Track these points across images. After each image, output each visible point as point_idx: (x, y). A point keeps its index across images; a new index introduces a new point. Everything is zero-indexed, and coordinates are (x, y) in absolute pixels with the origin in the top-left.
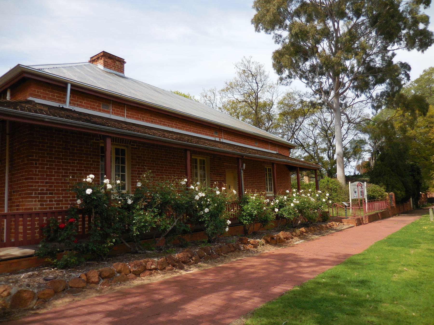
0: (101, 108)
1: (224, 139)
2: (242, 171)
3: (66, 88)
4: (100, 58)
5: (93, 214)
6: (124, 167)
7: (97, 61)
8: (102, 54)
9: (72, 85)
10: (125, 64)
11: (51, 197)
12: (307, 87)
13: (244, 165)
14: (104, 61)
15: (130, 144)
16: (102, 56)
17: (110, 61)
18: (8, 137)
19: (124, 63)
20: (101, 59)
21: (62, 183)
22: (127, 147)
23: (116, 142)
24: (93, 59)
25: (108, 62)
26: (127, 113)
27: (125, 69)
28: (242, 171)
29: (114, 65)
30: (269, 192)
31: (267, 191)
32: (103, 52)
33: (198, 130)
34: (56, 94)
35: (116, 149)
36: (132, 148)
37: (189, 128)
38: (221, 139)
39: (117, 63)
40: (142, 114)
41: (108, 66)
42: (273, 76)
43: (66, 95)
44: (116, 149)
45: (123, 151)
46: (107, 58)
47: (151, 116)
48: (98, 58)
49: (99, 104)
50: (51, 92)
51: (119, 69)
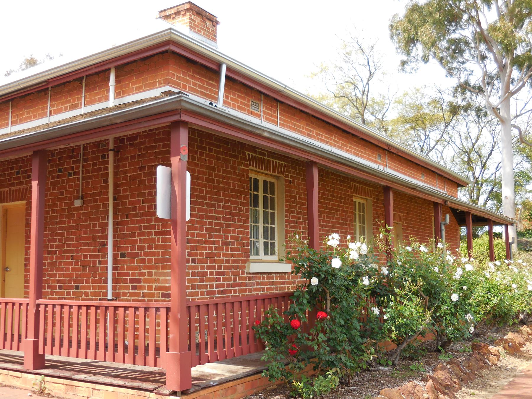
0: (250, 109)
1: (389, 167)
2: (443, 227)
3: (218, 73)
4: (183, 13)
5: (329, 302)
6: (274, 213)
7: (173, 18)
8: (187, 6)
9: (228, 69)
10: (218, 27)
11: (194, 266)
12: (447, 76)
13: (448, 216)
14: (190, 19)
15: (283, 174)
16: (187, 10)
17: (198, 19)
18: (111, 154)
19: (217, 23)
20: (184, 15)
21: (206, 242)
22: (277, 178)
23: (267, 170)
24: (168, 13)
25: (195, 21)
26: (281, 119)
27: (218, 35)
28: (443, 227)
29: (204, 26)
30: (261, 256)
31: (257, 254)
32: (190, 3)
33: (359, 151)
34: (197, 82)
35: (264, 181)
36: (286, 180)
37: (350, 147)
38: (385, 168)
39: (208, 23)
40: (297, 121)
41: (195, 29)
42: (389, 51)
43: (218, 87)
44: (264, 181)
45: (272, 184)
46: (194, 12)
47: (307, 125)
48: (178, 13)
49: (248, 101)
50: (193, 77)
51: (210, 33)
